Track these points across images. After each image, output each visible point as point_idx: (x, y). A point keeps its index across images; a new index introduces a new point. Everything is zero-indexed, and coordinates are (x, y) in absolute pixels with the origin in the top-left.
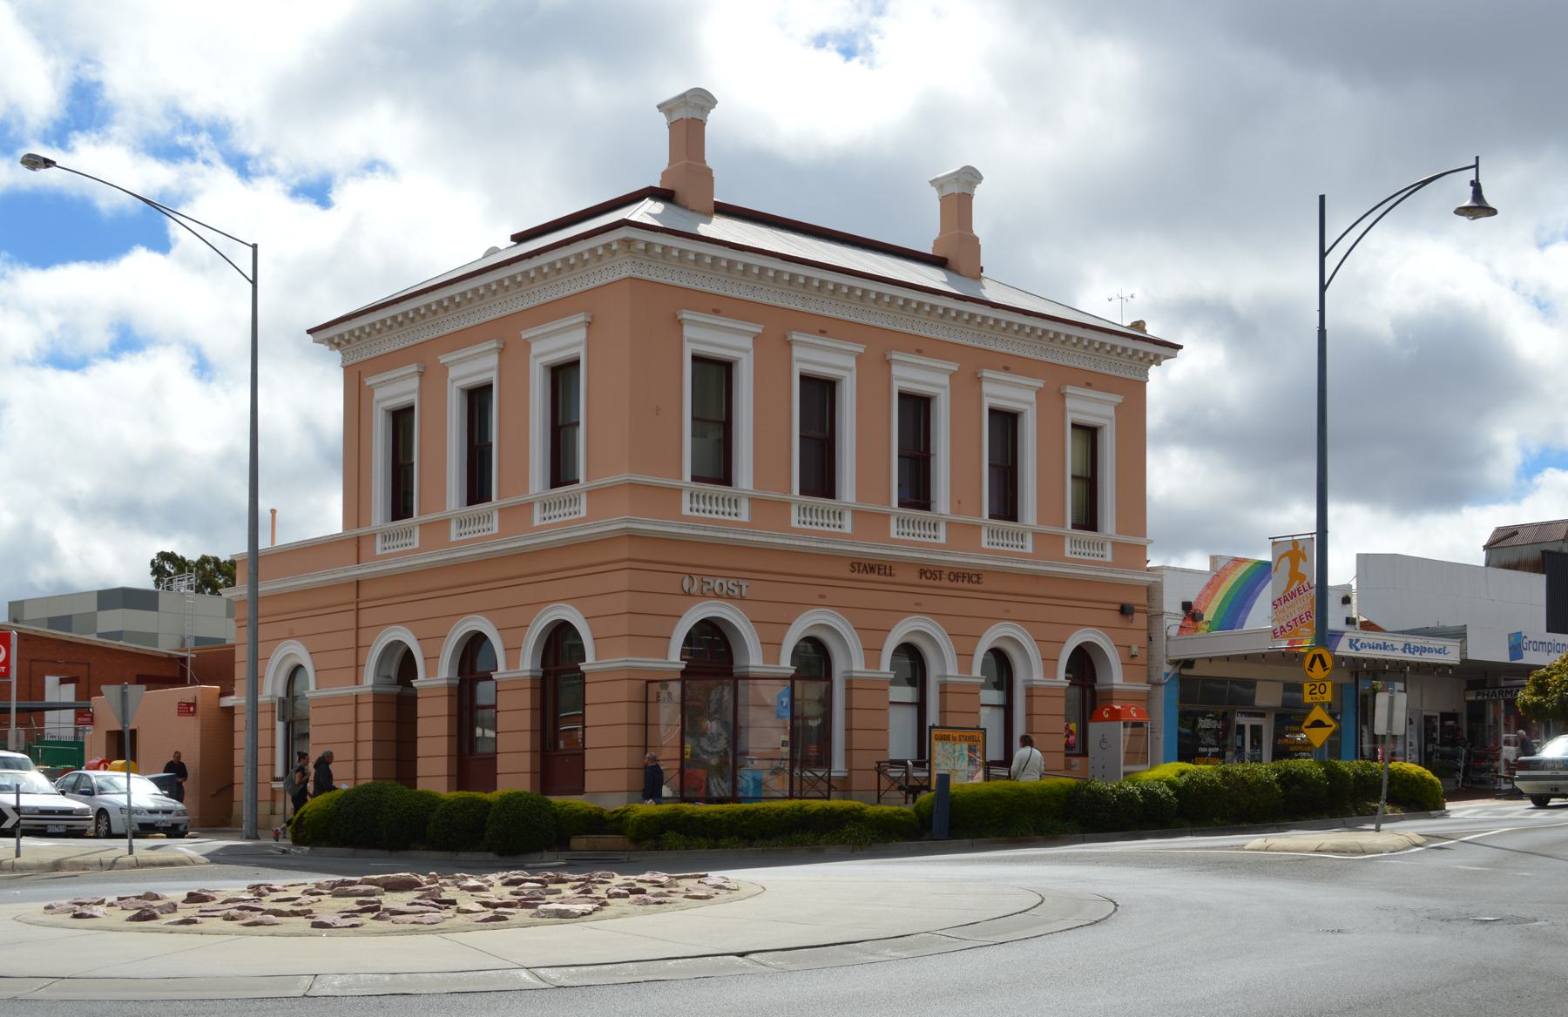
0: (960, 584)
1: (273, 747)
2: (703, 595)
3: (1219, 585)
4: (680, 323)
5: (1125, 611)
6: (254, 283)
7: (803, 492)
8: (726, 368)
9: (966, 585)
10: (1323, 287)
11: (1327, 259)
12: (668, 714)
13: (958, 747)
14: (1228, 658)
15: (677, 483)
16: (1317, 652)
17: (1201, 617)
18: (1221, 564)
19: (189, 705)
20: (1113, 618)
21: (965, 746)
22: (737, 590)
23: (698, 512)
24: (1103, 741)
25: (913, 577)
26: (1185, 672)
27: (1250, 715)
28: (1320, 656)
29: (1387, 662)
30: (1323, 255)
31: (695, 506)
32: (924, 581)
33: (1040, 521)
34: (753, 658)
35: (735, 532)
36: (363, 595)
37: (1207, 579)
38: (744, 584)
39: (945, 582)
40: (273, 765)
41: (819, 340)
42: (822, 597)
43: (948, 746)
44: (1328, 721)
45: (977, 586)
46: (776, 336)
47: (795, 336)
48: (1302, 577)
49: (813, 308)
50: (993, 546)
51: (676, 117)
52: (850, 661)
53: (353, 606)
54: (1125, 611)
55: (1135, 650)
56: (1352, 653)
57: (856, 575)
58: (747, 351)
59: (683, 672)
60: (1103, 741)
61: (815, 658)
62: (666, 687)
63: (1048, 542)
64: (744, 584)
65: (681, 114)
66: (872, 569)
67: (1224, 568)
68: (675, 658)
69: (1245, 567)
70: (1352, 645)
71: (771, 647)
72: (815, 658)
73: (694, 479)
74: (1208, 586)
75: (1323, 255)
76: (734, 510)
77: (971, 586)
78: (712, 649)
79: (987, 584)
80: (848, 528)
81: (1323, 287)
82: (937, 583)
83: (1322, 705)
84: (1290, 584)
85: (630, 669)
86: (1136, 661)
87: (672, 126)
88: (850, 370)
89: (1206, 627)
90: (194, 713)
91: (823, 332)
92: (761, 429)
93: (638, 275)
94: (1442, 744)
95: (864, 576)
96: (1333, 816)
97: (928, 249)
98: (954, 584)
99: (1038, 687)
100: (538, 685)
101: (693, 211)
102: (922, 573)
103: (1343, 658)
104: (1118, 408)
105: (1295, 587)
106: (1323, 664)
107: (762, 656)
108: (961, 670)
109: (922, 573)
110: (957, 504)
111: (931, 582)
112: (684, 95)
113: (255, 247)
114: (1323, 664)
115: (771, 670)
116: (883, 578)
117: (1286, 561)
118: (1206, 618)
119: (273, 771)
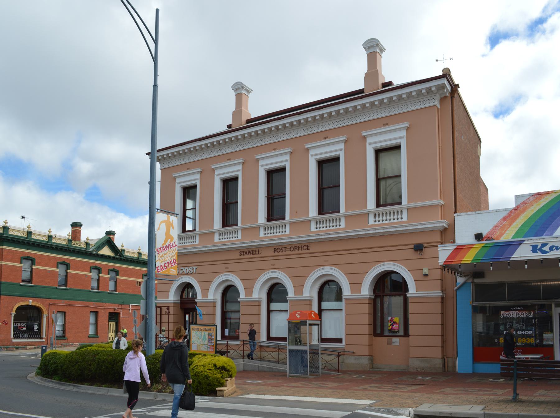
0: (297, 252)
5: (419, 248)
9: (300, 251)
13: (203, 334)
20: (411, 254)
21: (207, 333)
25: (271, 252)
26: (477, 281)
32: (276, 253)
38: (195, 268)
39: (288, 252)
42: (274, 265)
43: (198, 333)
49: (223, 152)
55: (426, 271)
56: (539, 256)
57: (242, 257)
66: (250, 253)
70: (535, 249)
71: (356, 285)
74: (505, 219)
77: (303, 251)
79: (264, 253)
82: (284, 253)
84: (166, 241)
86: (428, 278)
91: (229, 160)
94: (532, 331)
95: (246, 256)
98: (294, 252)
102: (275, 250)
105: (168, 243)
107: (209, 296)
108: (296, 293)
109: (275, 250)
111: (280, 253)
116: (255, 256)
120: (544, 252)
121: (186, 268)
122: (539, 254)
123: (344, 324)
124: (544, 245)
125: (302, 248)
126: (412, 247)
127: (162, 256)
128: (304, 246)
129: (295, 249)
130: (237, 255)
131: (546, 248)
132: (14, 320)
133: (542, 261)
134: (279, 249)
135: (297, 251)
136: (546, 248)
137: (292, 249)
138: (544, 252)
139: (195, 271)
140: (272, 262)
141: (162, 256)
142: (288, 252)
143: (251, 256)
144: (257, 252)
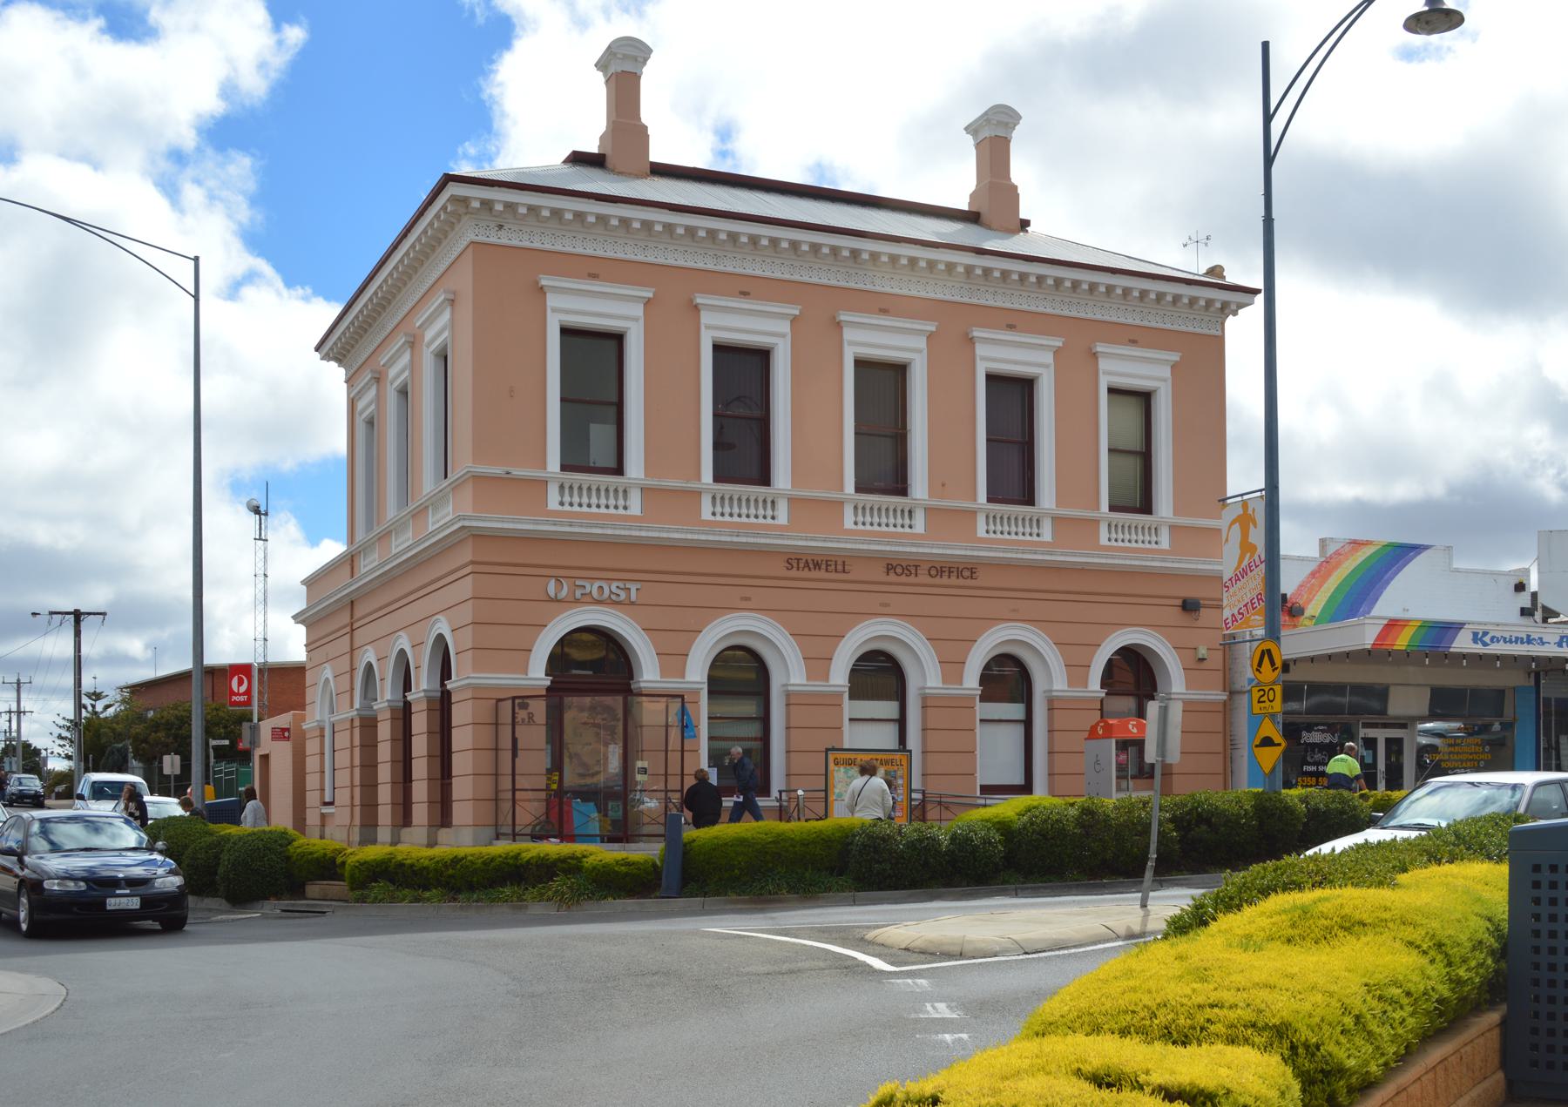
0: (945, 580)
1: (323, 772)
2: (577, 601)
3: (1329, 574)
4: (1095, 356)
5: (1189, 606)
6: (196, 297)
7: (718, 477)
8: (899, 371)
9: (954, 580)
10: (1269, 160)
11: (1273, 124)
12: (534, 737)
14: (1312, 659)
15: (967, 505)
16: (1265, 646)
17: (1301, 611)
18: (1331, 550)
19: (284, 730)
20: (1174, 615)
22: (623, 595)
23: (569, 506)
24: (1097, 762)
25: (878, 573)
27: (1385, 726)
28: (1269, 651)
29: (1533, 659)
30: (1268, 118)
31: (1114, 536)
32: (892, 577)
33: (1060, 501)
34: (649, 673)
35: (614, 527)
36: (357, 615)
37: (1312, 567)
38: (633, 587)
39: (923, 578)
40: (323, 790)
41: (744, 304)
44: (1278, 738)
45: (969, 582)
46: (675, 299)
47: (1100, 348)
48: (1253, 548)
50: (993, 534)
51: (612, 70)
52: (789, 673)
53: (348, 629)
54: (1189, 606)
55: (1203, 652)
56: (1478, 649)
58: (1047, 366)
59: (549, 689)
60: (1097, 762)
61: (741, 674)
62: (524, 706)
63: (1072, 527)
64: (633, 587)
65: (986, 133)
66: (817, 566)
67: (1337, 553)
68: (537, 673)
69: (1368, 551)
72: (741, 674)
73: (1112, 508)
74: (1313, 574)
75: (1268, 118)
76: (1154, 538)
77: (961, 582)
78: (594, 666)
79: (983, 579)
80: (1047, 536)
81: (1269, 160)
82: (912, 579)
83: (1273, 716)
85: (475, 688)
86: (1204, 665)
87: (978, 146)
88: (920, 351)
89: (1307, 622)
90: (288, 739)
92: (664, 410)
93: (481, 239)
95: (806, 574)
96: (949, 884)
97: (964, 205)
98: (937, 580)
99: (1060, 699)
100: (438, 706)
101: (620, 173)
102: (890, 568)
103: (1464, 656)
104: (1175, 367)
105: (1246, 562)
106: (1272, 663)
108: (664, 672)
109: (890, 568)
110: (938, 484)
111: (903, 579)
112: (986, 113)
113: (196, 259)
114: (1272, 663)
115: (1078, 693)
116: (833, 576)
117: (1236, 527)
118: (1308, 613)
119: (322, 795)
120: (1485, 644)
121: (597, 584)
122: (1480, 646)
123: (978, 752)
124: (1485, 634)
125: (960, 574)
126: (1179, 602)
127: (1235, 594)
128: (963, 570)
129: (940, 572)
130: (779, 568)
131: (1487, 639)
132: (120, 770)
133: (1480, 657)
134: (899, 567)
135: (953, 578)
136: (1487, 639)
137: (933, 572)
138: (1485, 644)
139: (633, 597)
140: (748, 592)
141: (1235, 594)
142: (923, 578)
143: (821, 574)
144: (840, 568)
